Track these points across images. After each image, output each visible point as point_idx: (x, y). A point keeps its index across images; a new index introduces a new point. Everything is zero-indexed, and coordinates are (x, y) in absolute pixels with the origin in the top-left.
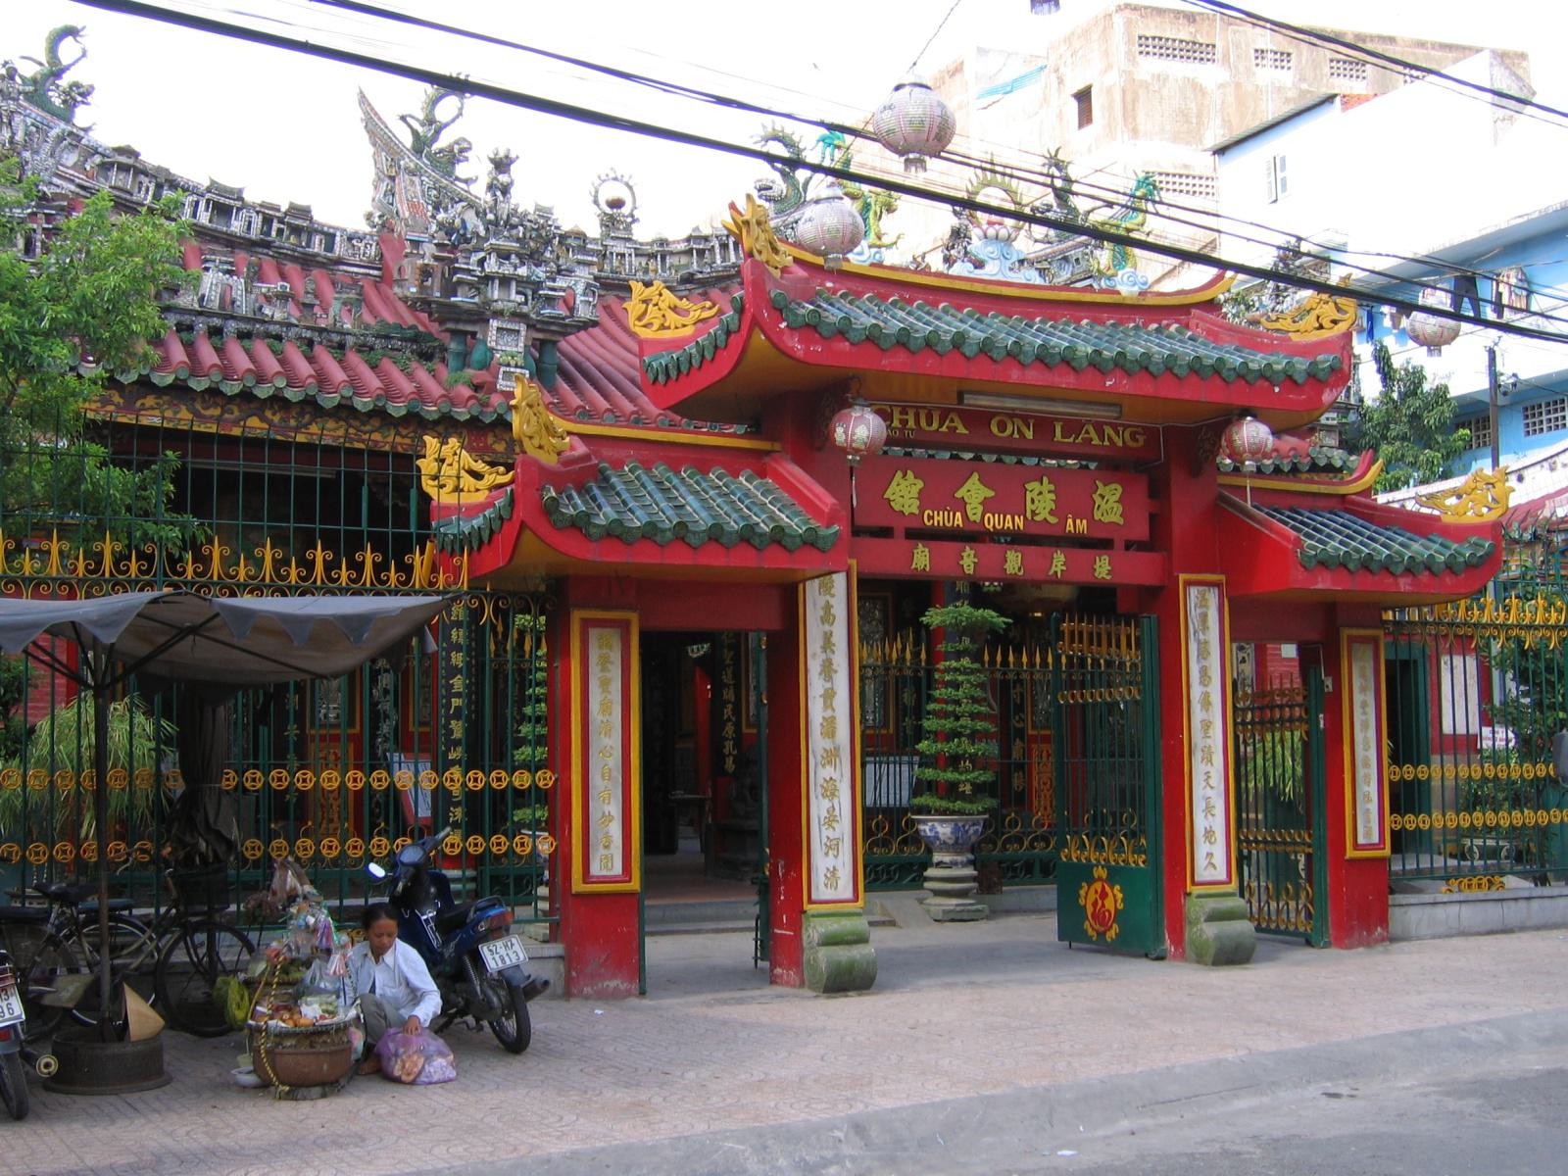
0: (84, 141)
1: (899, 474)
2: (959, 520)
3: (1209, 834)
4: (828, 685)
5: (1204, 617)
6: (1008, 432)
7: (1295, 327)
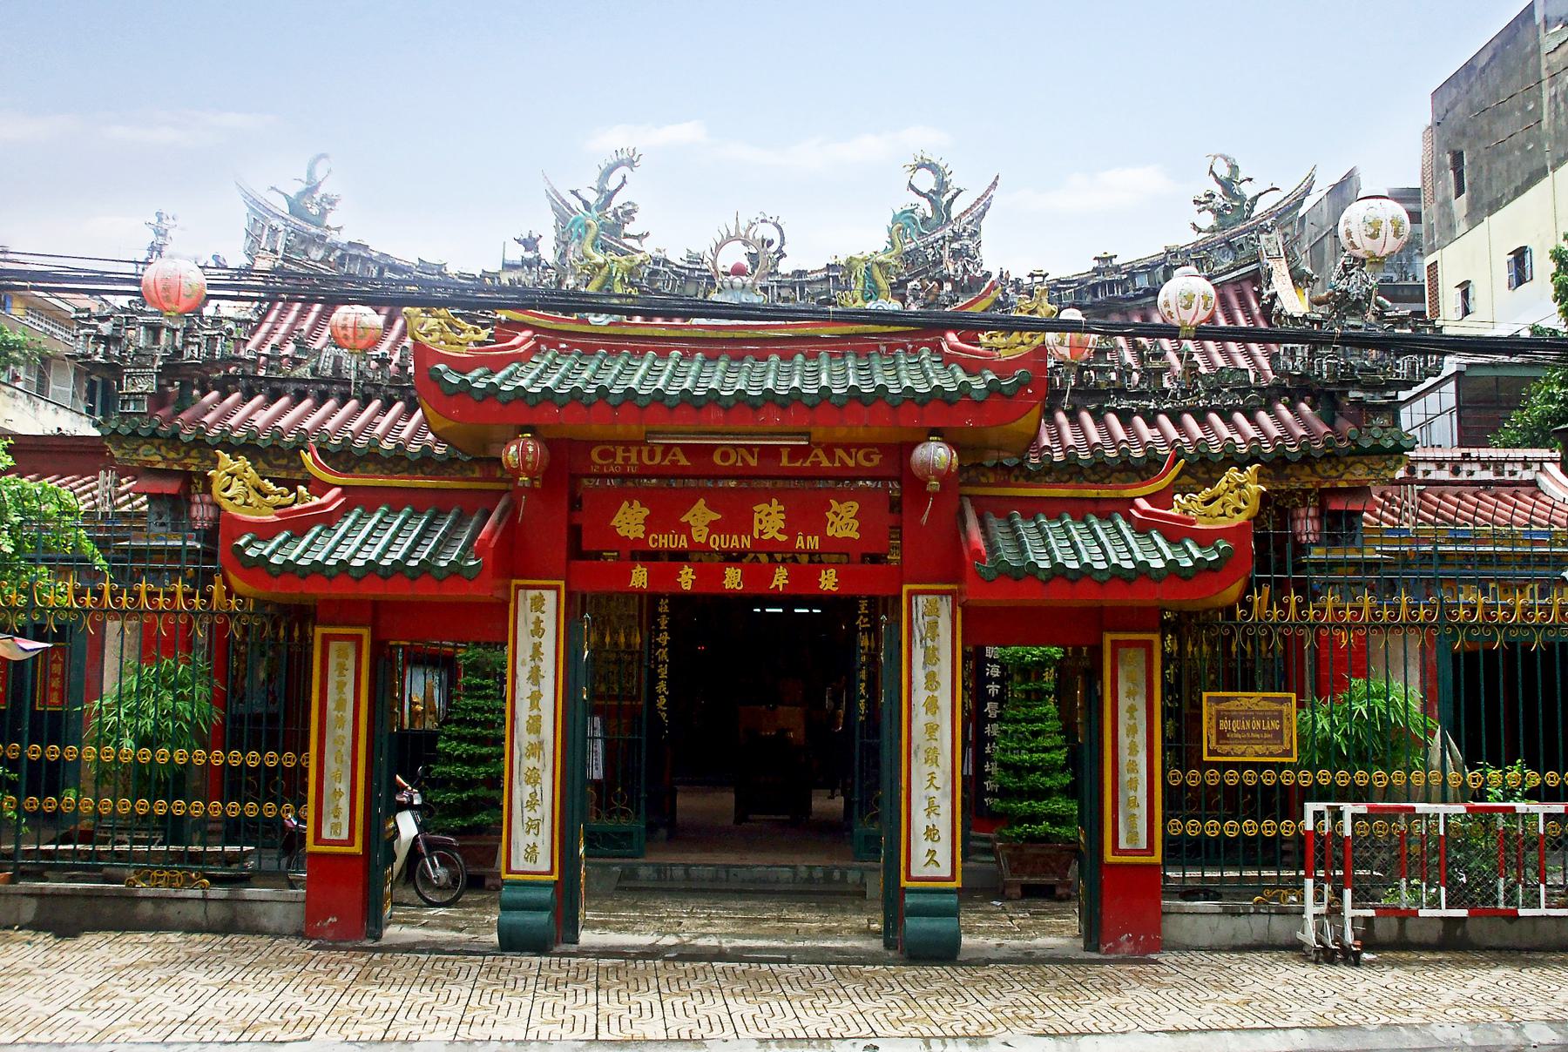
1: (626, 504)
3: (931, 833)
4: (535, 688)
5: (934, 626)
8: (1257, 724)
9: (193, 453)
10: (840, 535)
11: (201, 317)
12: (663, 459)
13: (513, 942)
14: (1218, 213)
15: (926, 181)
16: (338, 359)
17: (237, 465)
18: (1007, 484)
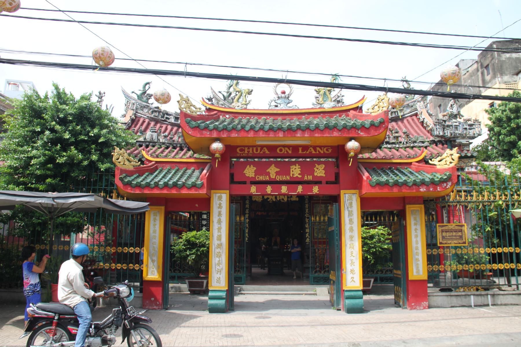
1: (248, 166)
2: (268, 178)
3: (352, 271)
5: (351, 204)
6: (283, 152)
7: (373, 111)
8: (454, 234)
10: (319, 175)
12: (261, 151)
16: (152, 135)
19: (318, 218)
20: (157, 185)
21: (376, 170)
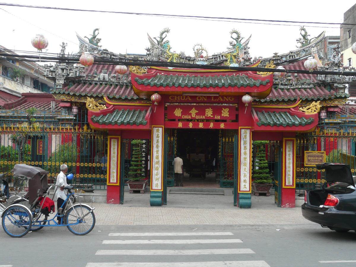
0: (98, 49)
1: (177, 109)
3: (245, 181)
4: (157, 149)
5: (246, 136)
6: (200, 100)
8: (317, 158)
9: (73, 97)
10: (224, 116)
11: (73, 67)
12: (185, 99)
13: (153, 204)
14: (302, 43)
15: (235, 36)
17: (91, 100)
18: (269, 105)
19: (227, 140)
20: (116, 122)
21: (264, 114)
